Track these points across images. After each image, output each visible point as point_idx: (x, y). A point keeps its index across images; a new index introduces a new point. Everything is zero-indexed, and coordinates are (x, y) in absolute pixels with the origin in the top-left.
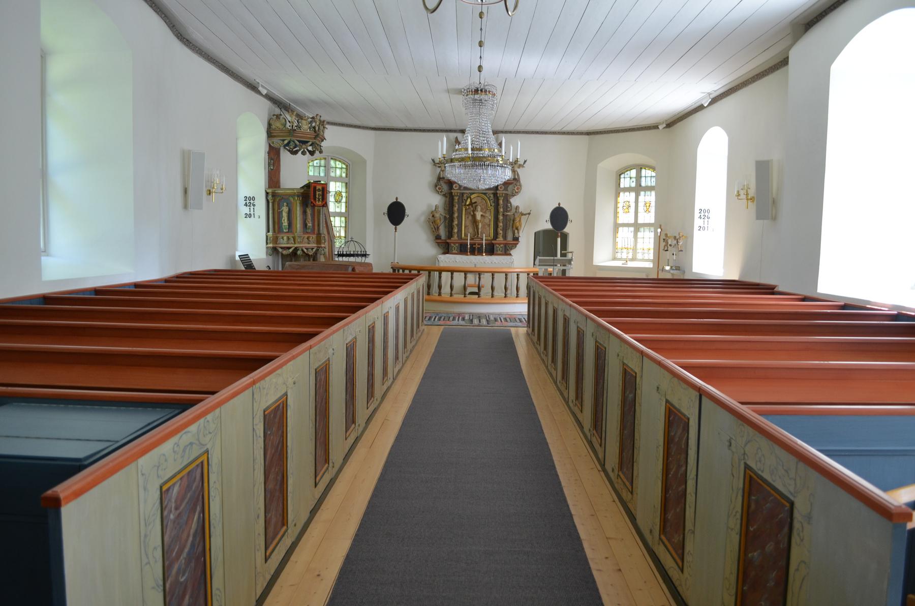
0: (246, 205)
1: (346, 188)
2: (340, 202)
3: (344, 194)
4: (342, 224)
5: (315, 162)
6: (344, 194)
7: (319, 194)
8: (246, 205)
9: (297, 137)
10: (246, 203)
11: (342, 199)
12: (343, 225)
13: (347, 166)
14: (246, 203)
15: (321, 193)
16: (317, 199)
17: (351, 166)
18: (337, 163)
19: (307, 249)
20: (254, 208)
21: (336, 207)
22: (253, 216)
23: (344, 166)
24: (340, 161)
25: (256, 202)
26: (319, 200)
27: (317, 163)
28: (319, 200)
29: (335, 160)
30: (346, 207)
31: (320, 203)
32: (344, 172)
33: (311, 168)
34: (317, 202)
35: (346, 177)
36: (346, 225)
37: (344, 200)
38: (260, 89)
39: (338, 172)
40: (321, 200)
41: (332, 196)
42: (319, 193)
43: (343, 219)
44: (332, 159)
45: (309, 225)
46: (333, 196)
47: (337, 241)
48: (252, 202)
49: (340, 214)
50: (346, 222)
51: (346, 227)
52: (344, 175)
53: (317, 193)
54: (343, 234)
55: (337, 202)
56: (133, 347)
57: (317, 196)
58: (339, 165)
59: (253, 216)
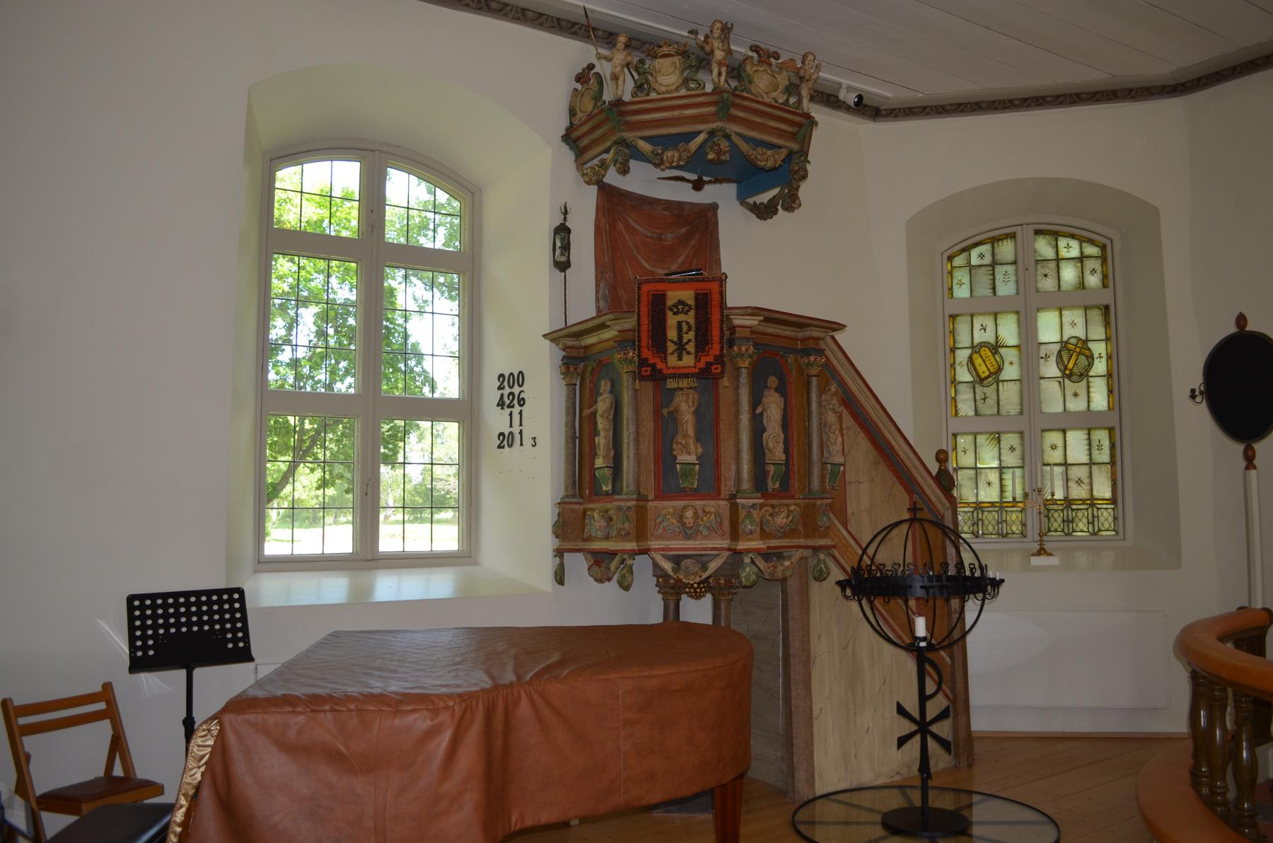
0: (501, 404)
1: (1107, 324)
2: (1084, 375)
3: (1099, 349)
4: (1095, 452)
5: (975, 253)
6: (1099, 349)
7: (679, 323)
8: (501, 404)
9: (639, 129)
10: (502, 395)
11: (1090, 365)
12: (1104, 456)
13: (1103, 248)
14: (502, 395)
15: (690, 318)
16: (671, 347)
17: (1118, 246)
18: (1062, 242)
19: (677, 560)
20: (521, 413)
21: (1069, 393)
22: (517, 437)
23: (1091, 250)
24: (1073, 236)
25: (528, 391)
26: (681, 347)
27: (981, 256)
28: (681, 347)
29: (1055, 235)
30: (1110, 391)
31: (688, 360)
32: (1093, 271)
33: (962, 276)
34: (672, 360)
35: (1105, 286)
36: (1112, 456)
37: (1100, 367)
38: (842, 95)
39: (1069, 274)
40: (691, 348)
41: (1047, 357)
42: (681, 317)
43: (1102, 436)
44: (1038, 232)
45: (683, 458)
46: (1053, 358)
47: (1080, 514)
48: (516, 390)
49: (1088, 422)
50: (1113, 446)
51: (1113, 462)
52: (1093, 281)
53: (672, 320)
54: (1103, 489)
55: (1069, 377)
56: (1201, 717)
57: (672, 334)
58: (1071, 249)
59: (517, 437)
